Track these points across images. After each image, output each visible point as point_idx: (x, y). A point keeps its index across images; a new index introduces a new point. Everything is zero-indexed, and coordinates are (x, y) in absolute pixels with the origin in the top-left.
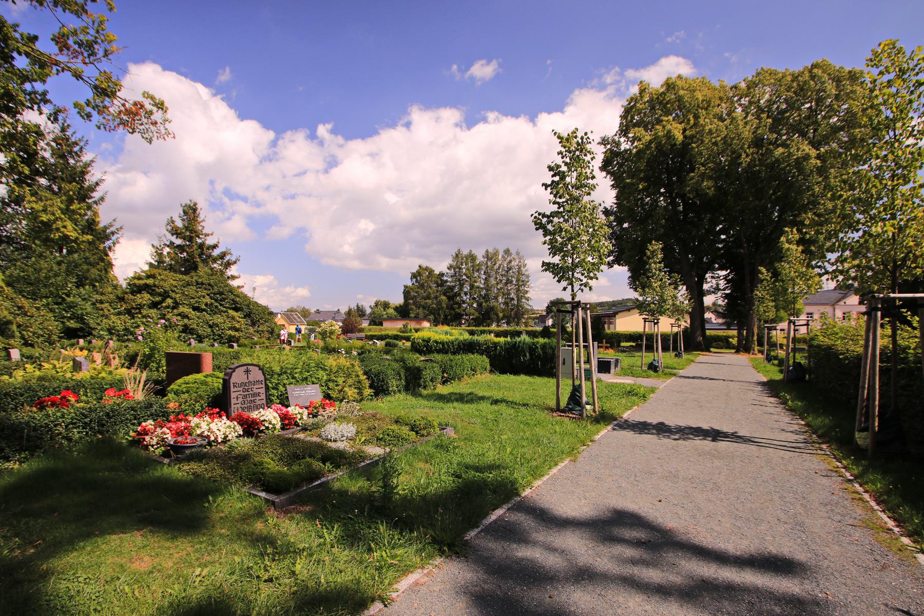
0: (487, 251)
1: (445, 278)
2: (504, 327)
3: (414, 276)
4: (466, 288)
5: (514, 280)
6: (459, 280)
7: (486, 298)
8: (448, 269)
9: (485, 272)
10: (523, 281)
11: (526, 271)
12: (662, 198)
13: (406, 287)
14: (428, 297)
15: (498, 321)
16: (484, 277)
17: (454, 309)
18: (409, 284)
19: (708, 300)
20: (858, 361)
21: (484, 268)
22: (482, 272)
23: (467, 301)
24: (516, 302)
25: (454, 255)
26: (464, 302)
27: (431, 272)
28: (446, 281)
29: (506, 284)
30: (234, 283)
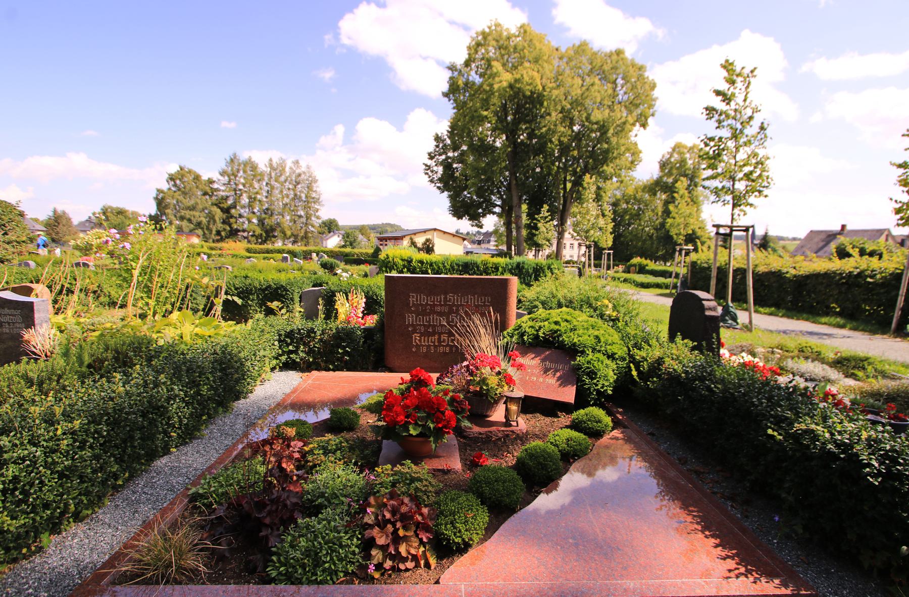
0: (271, 160)
1: (215, 186)
2: (290, 246)
3: (172, 178)
4: (245, 200)
5: (303, 196)
6: (235, 190)
7: (268, 212)
8: (221, 175)
9: (267, 184)
10: (313, 198)
11: (317, 187)
12: (311, 360)
13: (160, 191)
14: (193, 208)
15: (285, 237)
16: (266, 189)
17: (230, 225)
18: (165, 186)
19: (562, 186)
20: (709, 268)
21: (266, 179)
22: (264, 184)
23: (248, 222)
24: (304, 220)
25: (228, 159)
26: (241, 216)
27: (197, 178)
28: (217, 190)
29: (293, 199)
30: (712, 541)
